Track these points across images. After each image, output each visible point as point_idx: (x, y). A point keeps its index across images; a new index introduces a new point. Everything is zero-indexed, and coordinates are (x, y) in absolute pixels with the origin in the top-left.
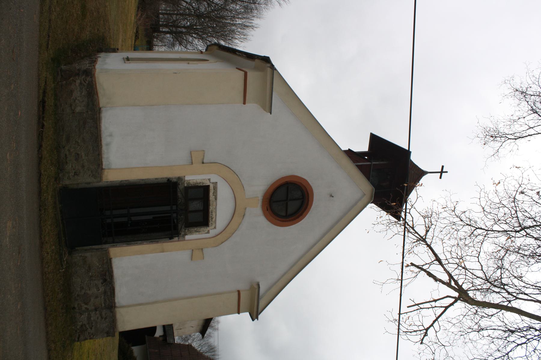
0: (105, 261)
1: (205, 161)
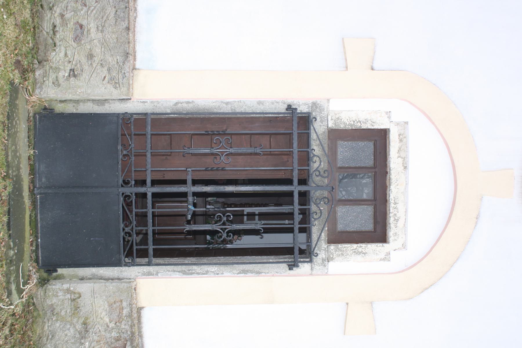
0: (125, 312)
1: (375, 66)
